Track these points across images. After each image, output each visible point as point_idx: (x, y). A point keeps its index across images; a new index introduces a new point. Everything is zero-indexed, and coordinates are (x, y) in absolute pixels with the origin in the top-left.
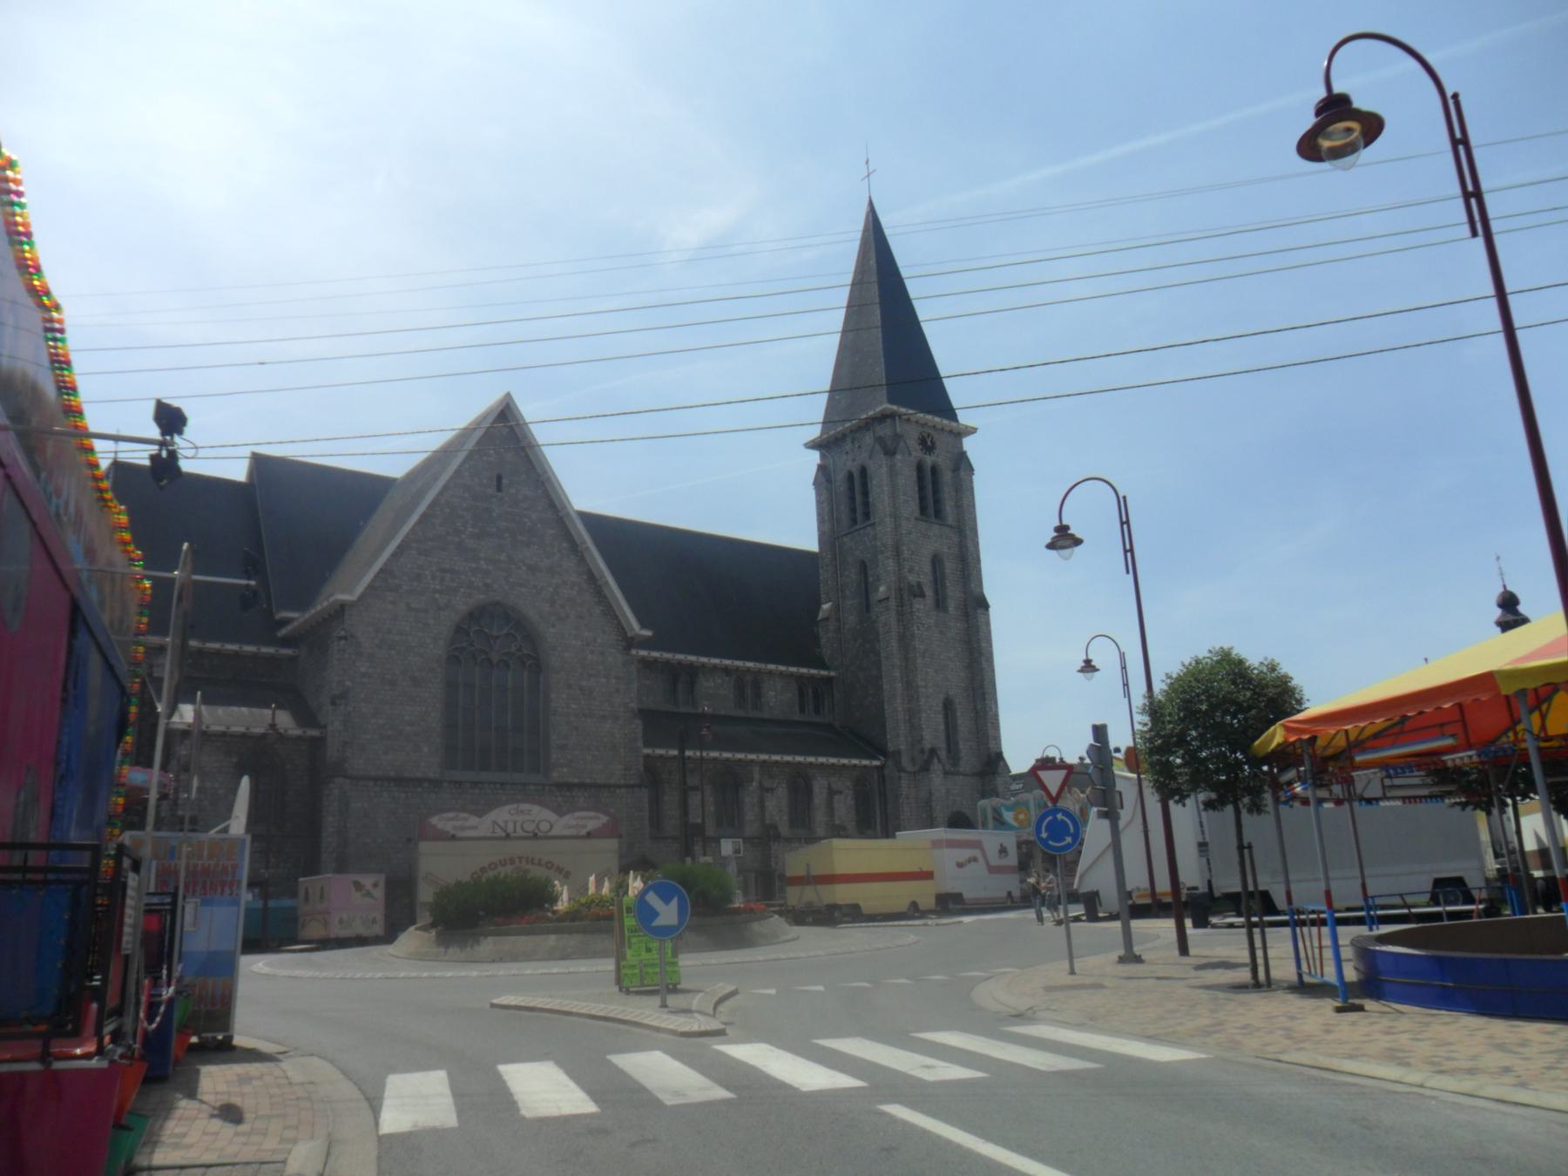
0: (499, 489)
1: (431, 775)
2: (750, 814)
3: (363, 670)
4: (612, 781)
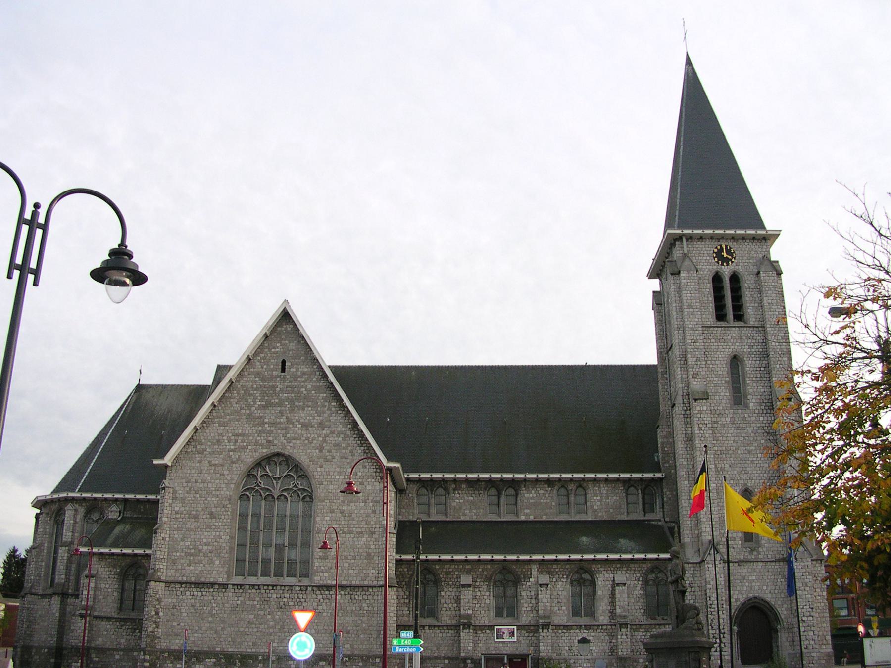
0: (283, 370)
1: (220, 580)
2: (525, 606)
3: (177, 509)
4: (366, 583)
